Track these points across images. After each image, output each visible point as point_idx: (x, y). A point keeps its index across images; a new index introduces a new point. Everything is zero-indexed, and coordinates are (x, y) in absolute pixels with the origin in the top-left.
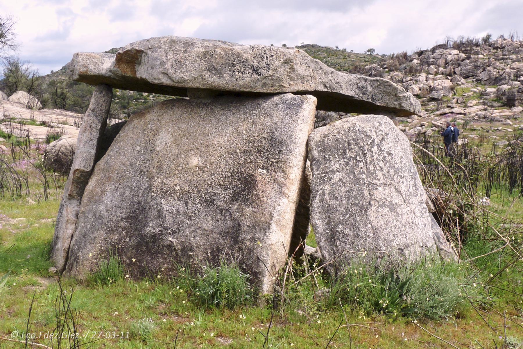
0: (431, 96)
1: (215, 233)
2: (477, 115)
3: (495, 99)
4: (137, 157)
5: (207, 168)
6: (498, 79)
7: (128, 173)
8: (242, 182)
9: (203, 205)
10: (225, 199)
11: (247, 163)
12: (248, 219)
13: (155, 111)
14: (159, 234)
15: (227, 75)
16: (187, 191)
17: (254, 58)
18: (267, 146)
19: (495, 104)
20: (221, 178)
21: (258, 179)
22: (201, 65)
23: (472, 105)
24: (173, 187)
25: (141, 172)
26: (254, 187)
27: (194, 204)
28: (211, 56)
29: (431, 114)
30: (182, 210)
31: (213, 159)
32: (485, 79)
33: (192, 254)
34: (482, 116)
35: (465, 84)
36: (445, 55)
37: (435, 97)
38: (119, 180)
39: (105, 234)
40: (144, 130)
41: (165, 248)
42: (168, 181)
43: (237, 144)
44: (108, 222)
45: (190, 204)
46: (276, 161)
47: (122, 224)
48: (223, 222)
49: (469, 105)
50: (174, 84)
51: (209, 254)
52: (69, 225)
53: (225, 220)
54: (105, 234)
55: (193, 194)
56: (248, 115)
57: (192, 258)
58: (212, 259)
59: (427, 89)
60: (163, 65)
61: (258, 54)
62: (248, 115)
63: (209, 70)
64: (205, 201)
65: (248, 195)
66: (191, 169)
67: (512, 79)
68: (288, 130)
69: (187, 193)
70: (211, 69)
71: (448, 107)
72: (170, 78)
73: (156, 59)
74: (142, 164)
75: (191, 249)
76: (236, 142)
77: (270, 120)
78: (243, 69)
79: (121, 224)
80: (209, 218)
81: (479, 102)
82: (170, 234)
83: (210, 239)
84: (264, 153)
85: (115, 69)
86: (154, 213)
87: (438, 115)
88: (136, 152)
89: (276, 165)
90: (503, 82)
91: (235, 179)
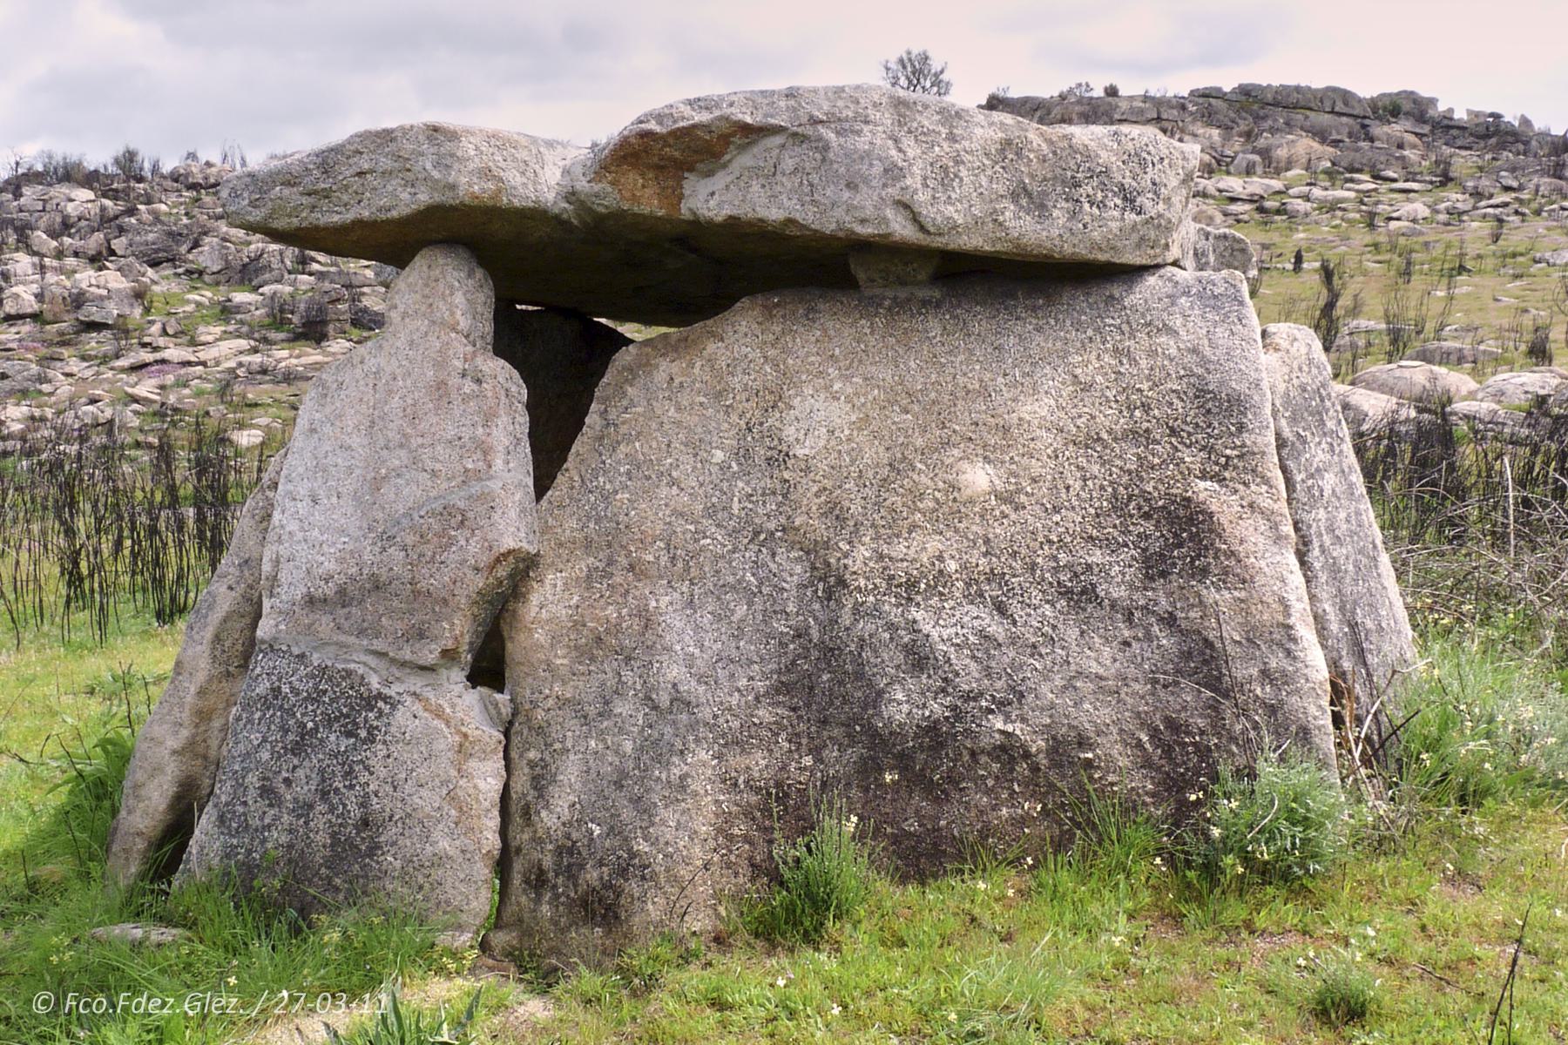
0: (82, 318)
1: (1136, 680)
2: (240, 365)
3: (267, 321)
4: (725, 485)
5: (1027, 494)
6: (251, 267)
7: (709, 541)
8: (1158, 522)
9: (1058, 606)
10: (1128, 578)
11: (1152, 468)
12: (1228, 624)
13: (743, 329)
14: (947, 718)
15: (1059, 214)
16: (988, 570)
17: (1124, 162)
18: (1192, 413)
19: (272, 335)
20: (1083, 518)
21: (1213, 508)
22: (995, 181)
23: (210, 338)
24: (934, 565)
25: (757, 534)
26: (1211, 531)
27: (1029, 606)
28: (1017, 154)
29: (102, 368)
30: (997, 628)
31: (1036, 468)
32: (215, 268)
33: (1090, 755)
34: (255, 367)
35: (162, 283)
36: (55, 202)
37: (97, 318)
38: (687, 569)
39: (714, 757)
40: (719, 395)
41: (984, 759)
42: (899, 550)
43: (1093, 417)
44: (715, 717)
45: (1015, 607)
46: (1235, 452)
47: (764, 714)
48: (1145, 646)
49: (203, 338)
50: (921, 236)
51: (1147, 746)
52: (473, 764)
53: (1149, 637)
54: (714, 757)
55: (1014, 576)
56: (1090, 332)
57: (1098, 767)
58: (1161, 758)
59: (64, 298)
60: (896, 179)
61: (1133, 152)
62: (1090, 332)
63: (1014, 197)
64: (1060, 593)
65: (1199, 556)
66: (971, 501)
67: (290, 268)
68: (1243, 367)
69: (991, 576)
70: (1019, 193)
71: (144, 345)
72: (915, 219)
73: (866, 156)
74: (750, 506)
75: (1083, 742)
76: (1086, 410)
77: (1172, 343)
78: (1100, 195)
79: (760, 713)
80: (1096, 639)
81: (225, 332)
82: (992, 711)
83: (1130, 700)
84: (1190, 434)
85: (597, 187)
86: (891, 658)
87: (123, 370)
88: (714, 469)
89: (1241, 464)
90: (267, 276)
91: (1131, 516)
